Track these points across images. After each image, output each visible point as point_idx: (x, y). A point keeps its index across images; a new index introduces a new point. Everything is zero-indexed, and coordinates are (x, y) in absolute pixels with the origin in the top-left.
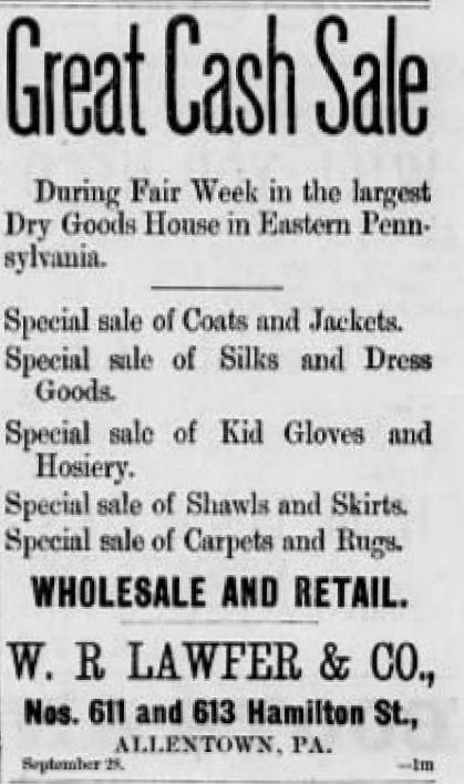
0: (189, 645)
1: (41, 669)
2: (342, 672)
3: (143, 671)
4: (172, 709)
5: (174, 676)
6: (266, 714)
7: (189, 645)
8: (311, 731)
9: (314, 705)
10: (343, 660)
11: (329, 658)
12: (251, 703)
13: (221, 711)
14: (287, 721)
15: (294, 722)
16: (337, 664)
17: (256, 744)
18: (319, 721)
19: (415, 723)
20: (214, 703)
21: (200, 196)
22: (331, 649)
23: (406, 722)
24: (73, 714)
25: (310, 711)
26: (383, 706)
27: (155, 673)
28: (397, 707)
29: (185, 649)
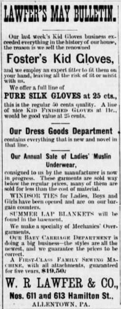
0: (53, 279)
1: (14, 285)
2: (93, 286)
3: (41, 285)
4: (48, 295)
5: (49, 287)
6: (73, 296)
7: (53, 279)
8: (83, 300)
9: (86, 294)
10: (94, 283)
11: (90, 282)
12: (69, 293)
13: (61, 296)
14: (79, 298)
15: (81, 298)
16: (92, 283)
17: (70, 304)
18: (87, 298)
19: (112, 298)
20: (59, 294)
21: (11, 88)
22: (90, 280)
23: (110, 298)
24: (22, 296)
25: (85, 295)
26: (104, 294)
27: (44, 286)
28: (108, 294)
29: (52, 280)
